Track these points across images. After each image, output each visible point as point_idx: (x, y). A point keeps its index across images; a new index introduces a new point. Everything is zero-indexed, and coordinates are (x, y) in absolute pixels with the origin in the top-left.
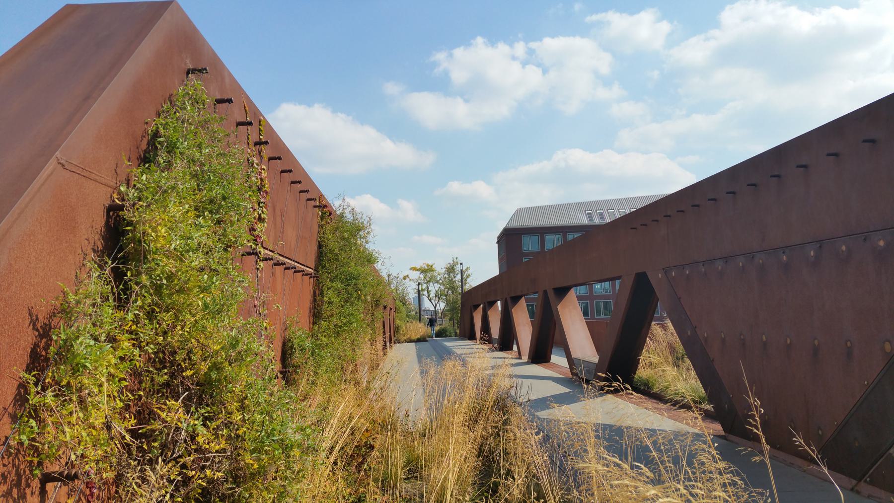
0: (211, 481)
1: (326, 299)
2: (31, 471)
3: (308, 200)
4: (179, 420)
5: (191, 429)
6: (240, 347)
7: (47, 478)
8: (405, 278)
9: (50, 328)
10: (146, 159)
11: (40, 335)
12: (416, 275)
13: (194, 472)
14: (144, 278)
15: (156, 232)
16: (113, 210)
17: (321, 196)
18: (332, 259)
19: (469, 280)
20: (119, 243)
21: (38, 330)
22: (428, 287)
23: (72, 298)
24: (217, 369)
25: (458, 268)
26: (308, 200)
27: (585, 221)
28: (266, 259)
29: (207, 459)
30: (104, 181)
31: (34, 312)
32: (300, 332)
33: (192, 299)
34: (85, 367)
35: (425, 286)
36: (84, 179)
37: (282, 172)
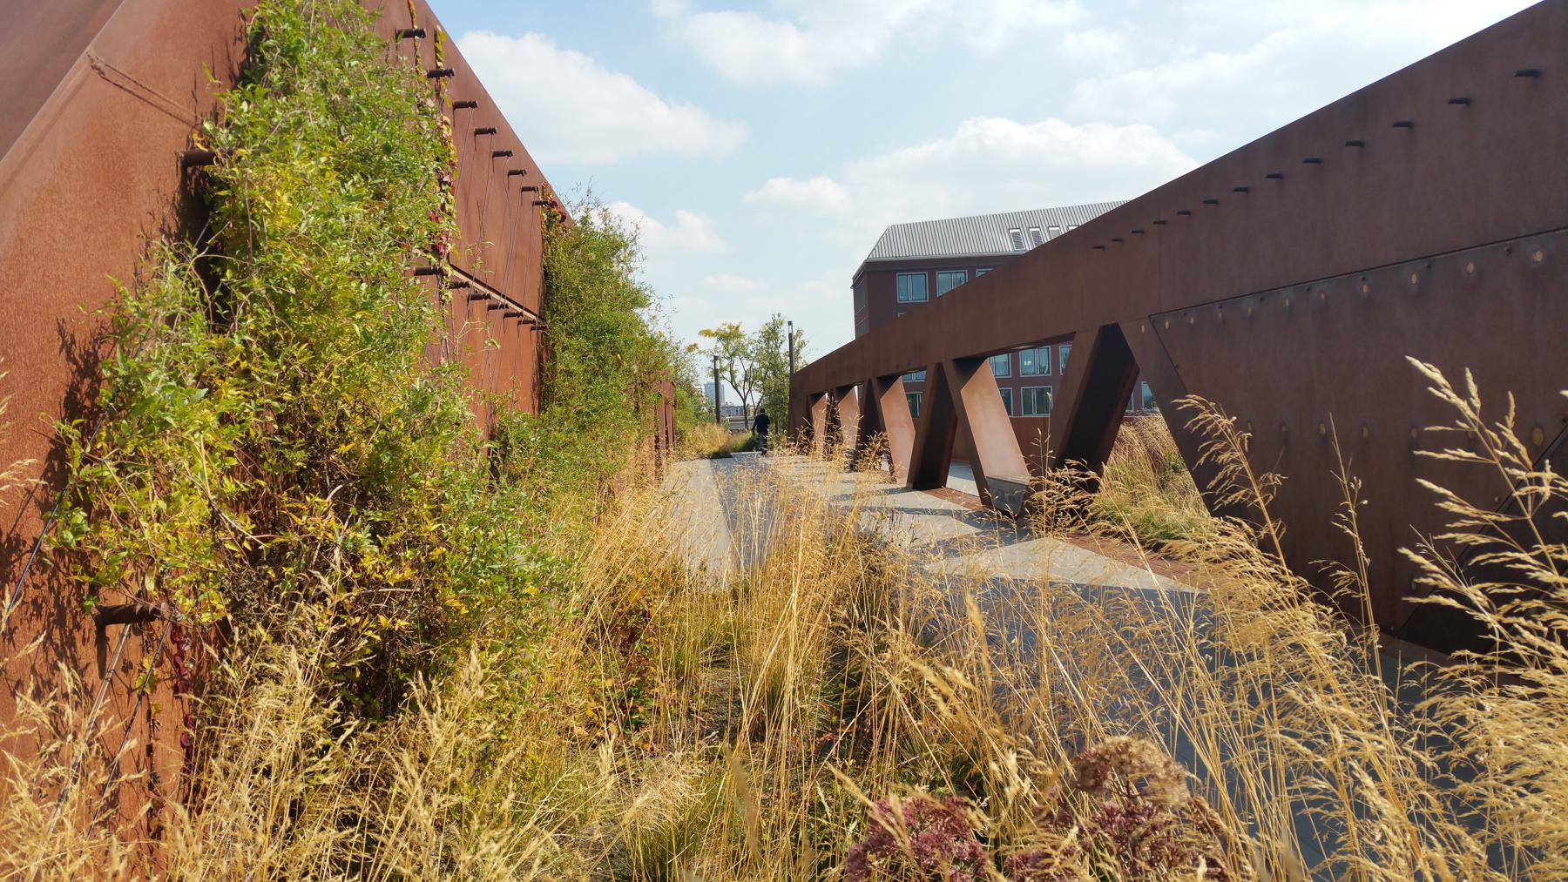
0: (389, 634)
1: (560, 367)
2: (80, 602)
3: (524, 189)
4: (330, 530)
5: (350, 545)
6: (429, 411)
7: (108, 616)
9: (97, 361)
10: (247, 74)
11: (79, 370)
12: (710, 344)
13: (358, 619)
14: (257, 283)
15: (272, 200)
16: (193, 162)
17: (546, 187)
18: (569, 303)
19: (803, 352)
20: (207, 215)
21: (75, 362)
22: (731, 365)
23: (131, 304)
24: (391, 448)
25: (784, 331)
26: (524, 189)
27: (1008, 247)
28: (457, 285)
29: (380, 598)
30: (172, 109)
31: (67, 327)
32: (519, 414)
33: (342, 321)
34: (165, 424)
35: (725, 363)
36: (138, 102)
37: (478, 132)
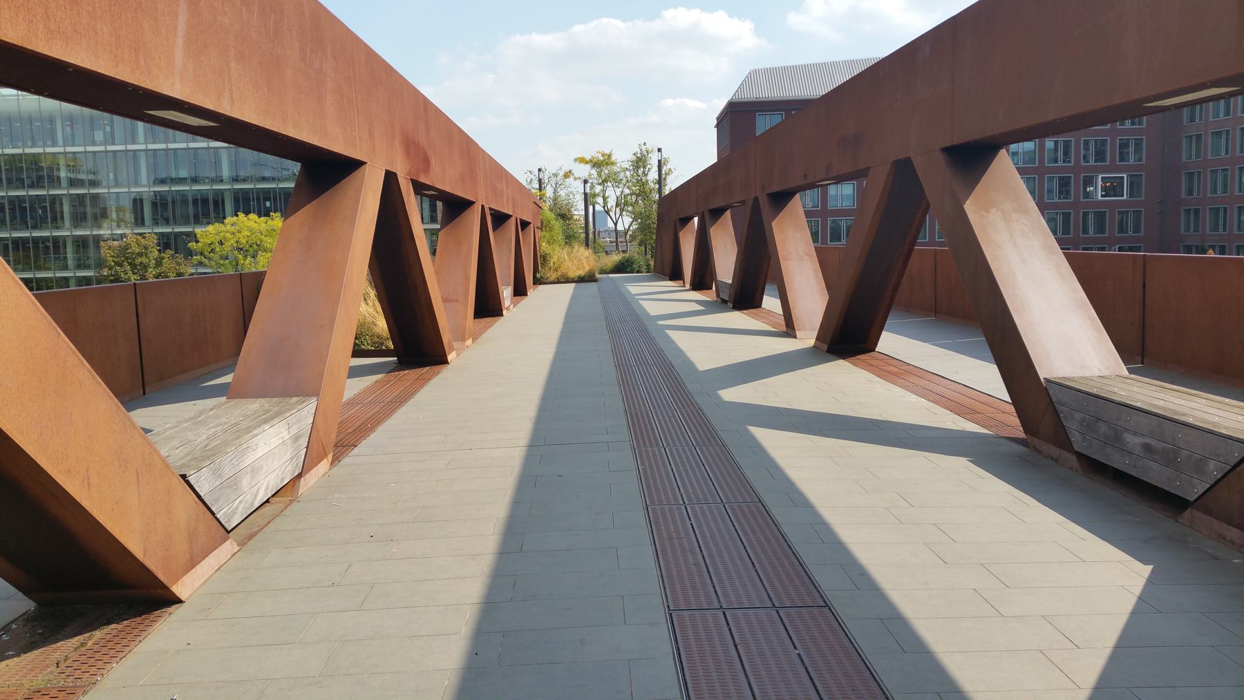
8: (566, 176)
12: (584, 171)
22: (604, 191)
25: (653, 160)
